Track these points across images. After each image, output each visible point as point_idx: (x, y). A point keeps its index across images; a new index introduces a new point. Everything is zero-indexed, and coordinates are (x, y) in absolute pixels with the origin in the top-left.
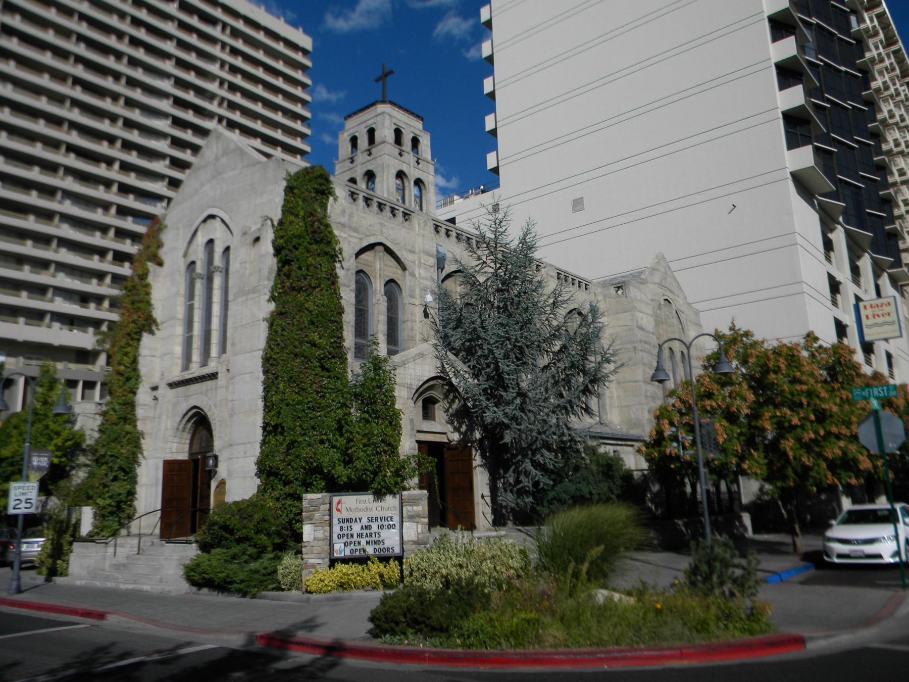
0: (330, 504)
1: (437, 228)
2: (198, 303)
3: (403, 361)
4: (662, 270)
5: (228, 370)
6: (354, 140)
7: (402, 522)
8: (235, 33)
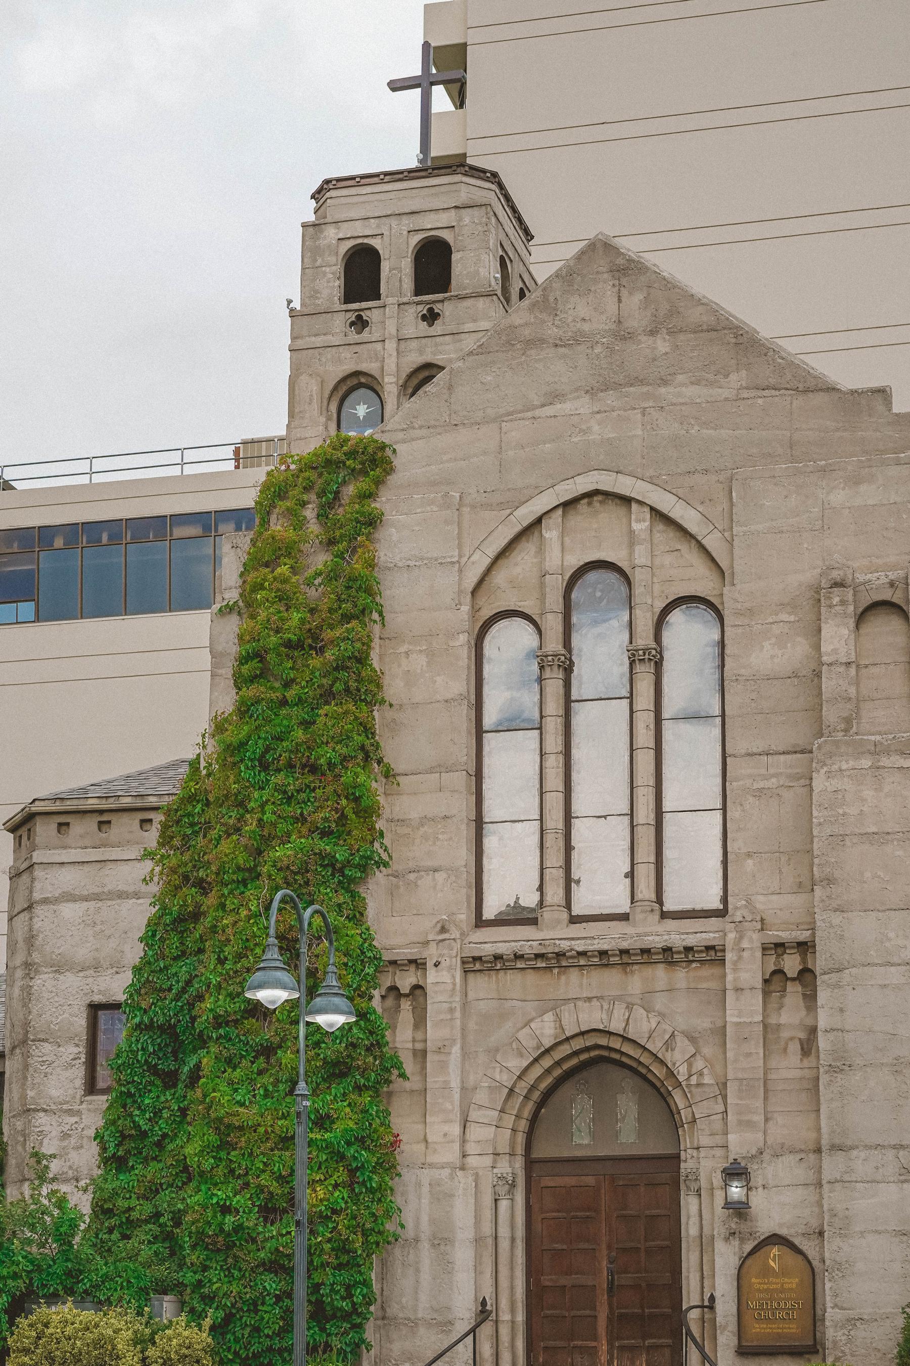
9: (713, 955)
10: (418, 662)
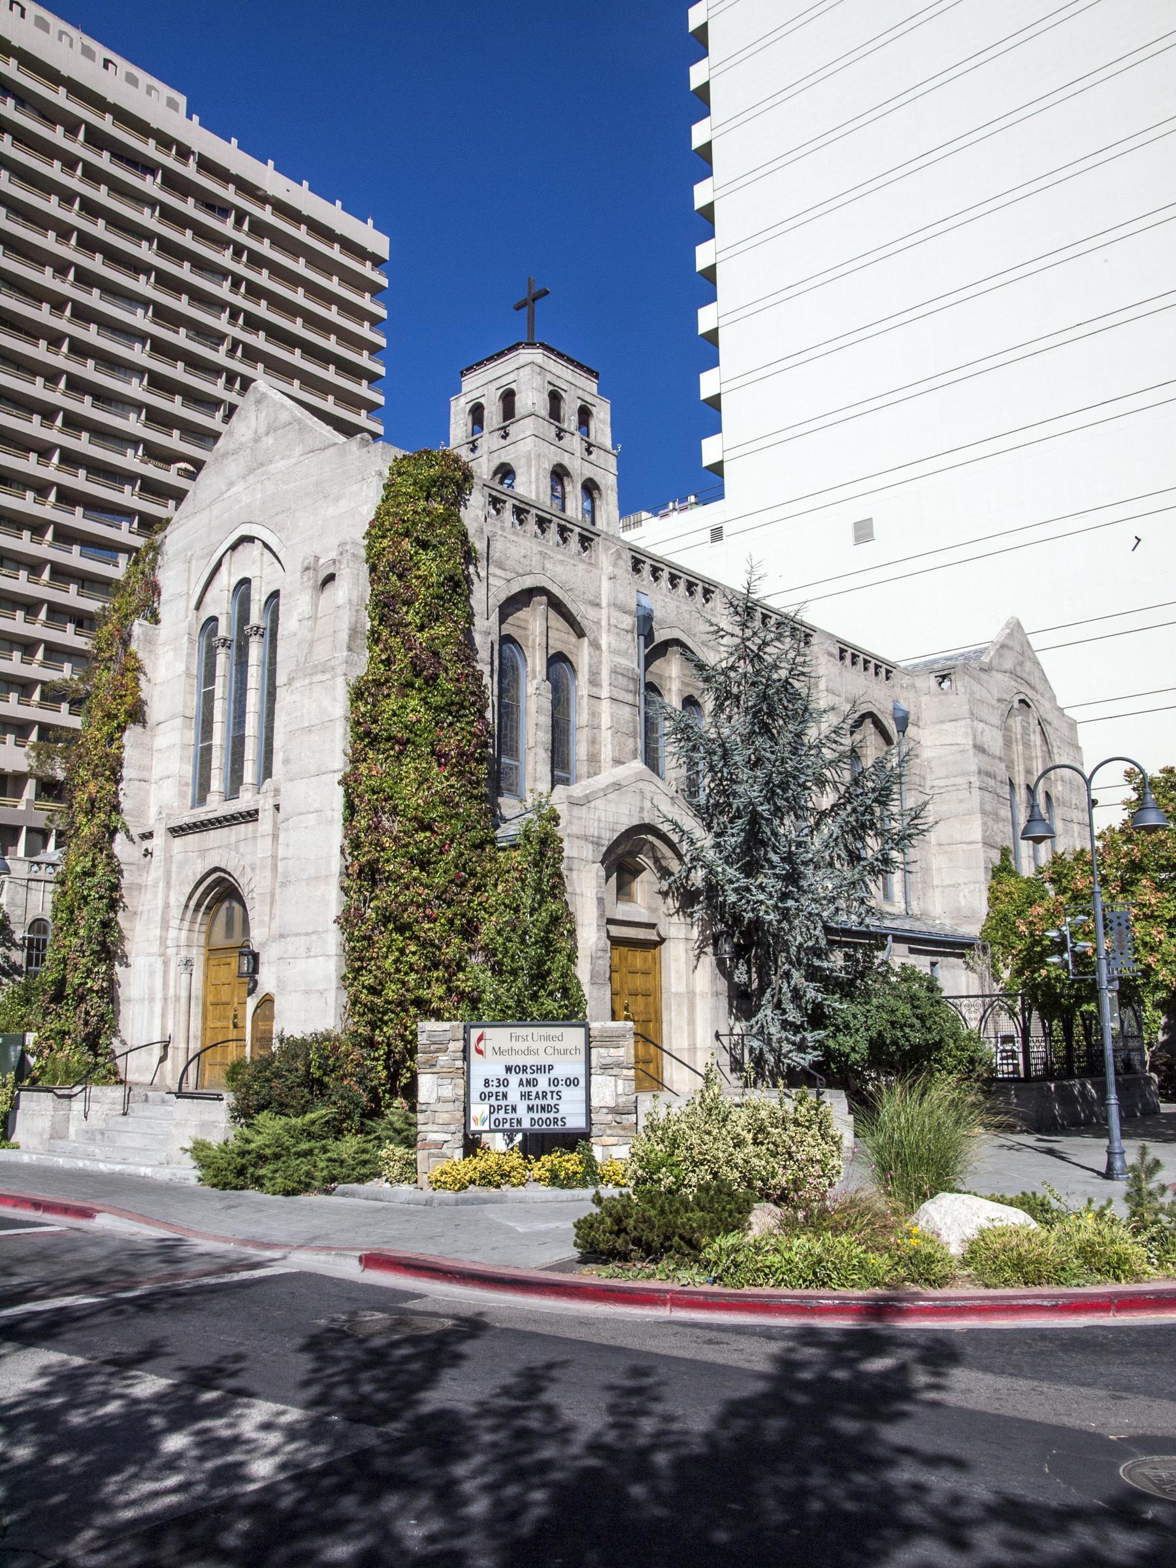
0: (466, 1041)
1: (637, 566)
2: (220, 688)
3: (587, 796)
4: (1018, 648)
5: (277, 807)
6: (477, 412)
7: (589, 1075)
8: (259, 229)
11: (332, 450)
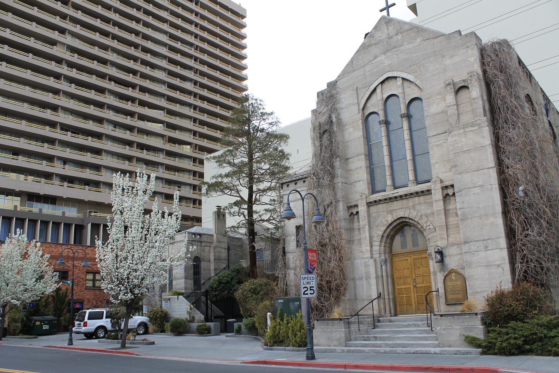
9: (429, 192)
10: (351, 130)
11: (442, 38)
